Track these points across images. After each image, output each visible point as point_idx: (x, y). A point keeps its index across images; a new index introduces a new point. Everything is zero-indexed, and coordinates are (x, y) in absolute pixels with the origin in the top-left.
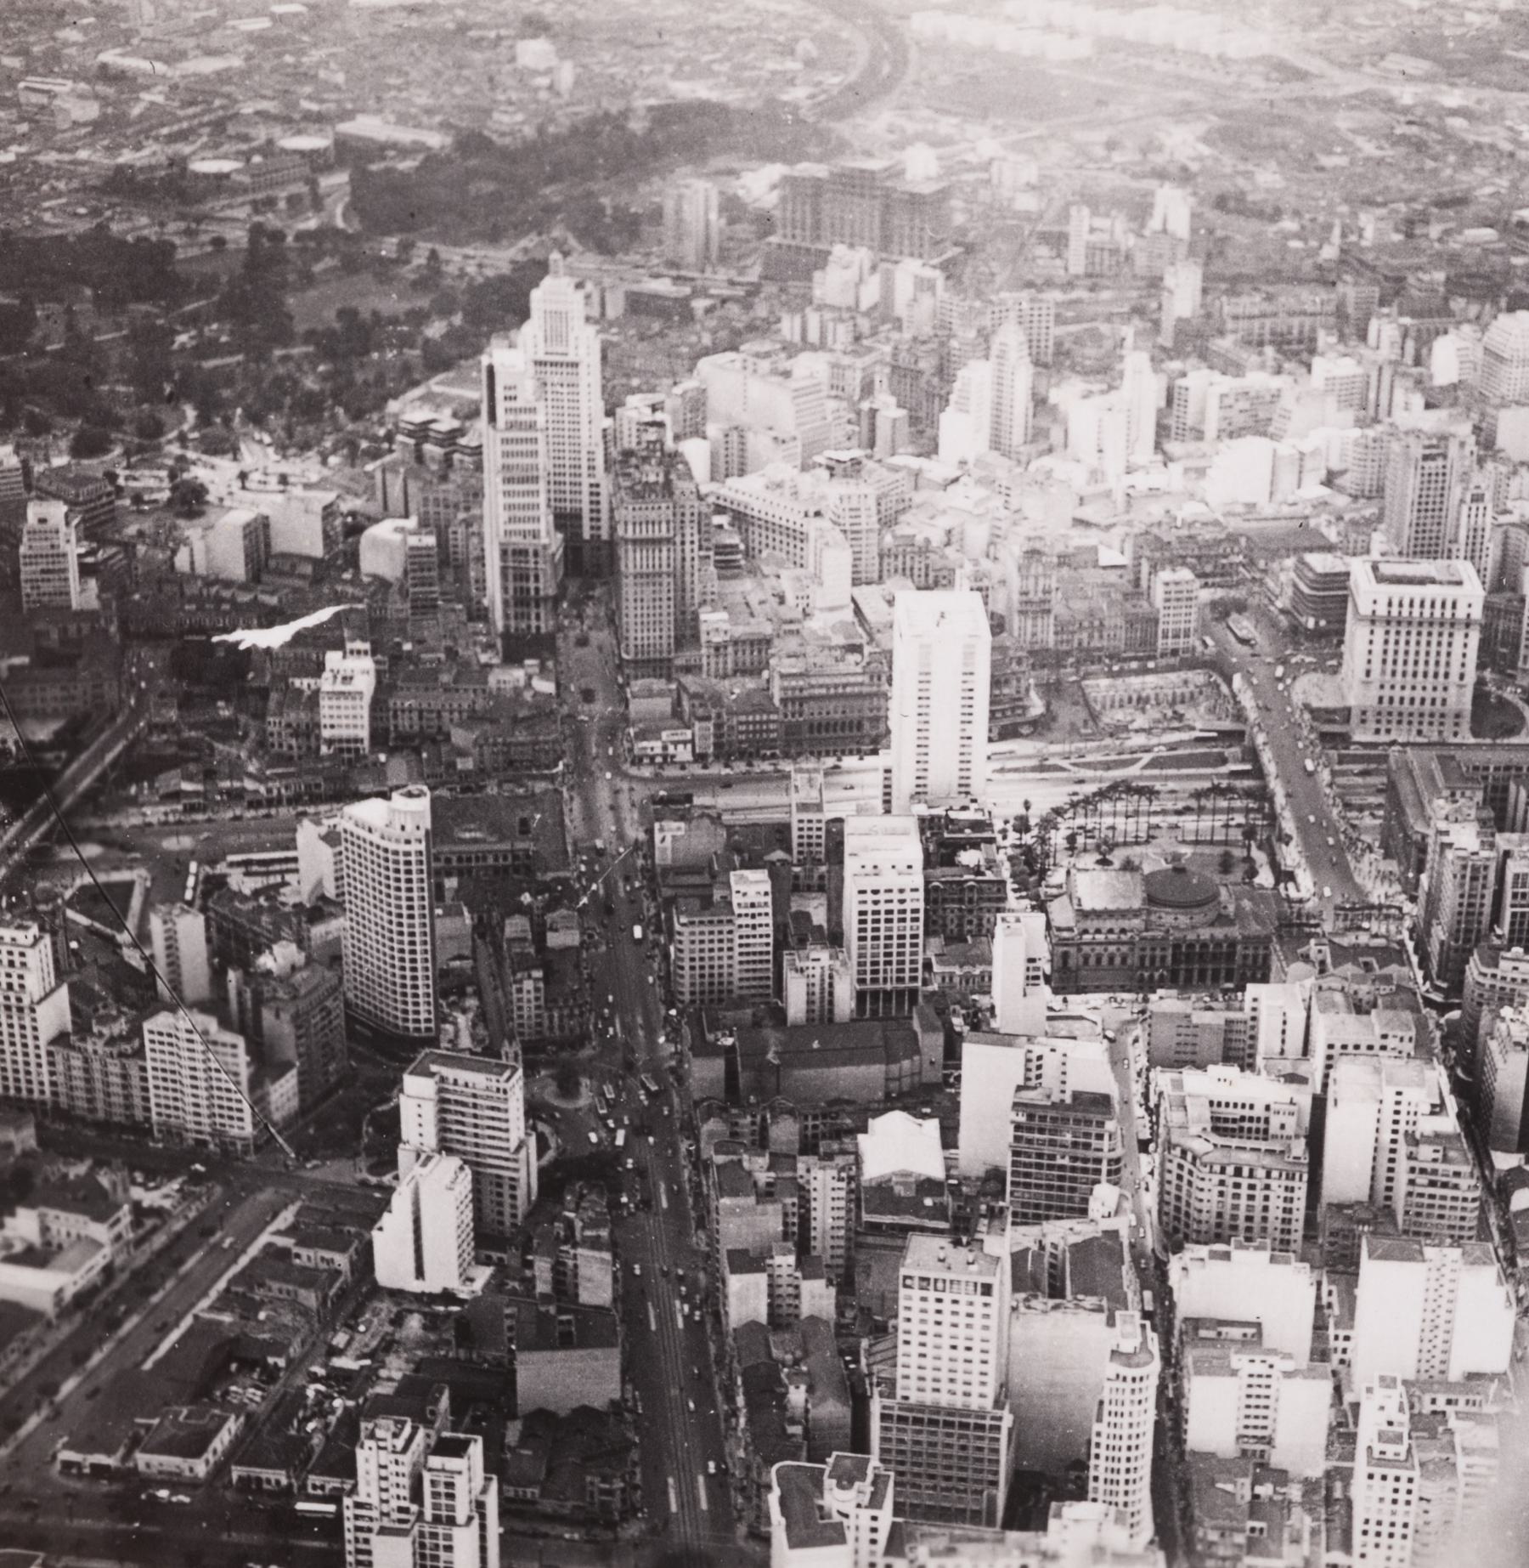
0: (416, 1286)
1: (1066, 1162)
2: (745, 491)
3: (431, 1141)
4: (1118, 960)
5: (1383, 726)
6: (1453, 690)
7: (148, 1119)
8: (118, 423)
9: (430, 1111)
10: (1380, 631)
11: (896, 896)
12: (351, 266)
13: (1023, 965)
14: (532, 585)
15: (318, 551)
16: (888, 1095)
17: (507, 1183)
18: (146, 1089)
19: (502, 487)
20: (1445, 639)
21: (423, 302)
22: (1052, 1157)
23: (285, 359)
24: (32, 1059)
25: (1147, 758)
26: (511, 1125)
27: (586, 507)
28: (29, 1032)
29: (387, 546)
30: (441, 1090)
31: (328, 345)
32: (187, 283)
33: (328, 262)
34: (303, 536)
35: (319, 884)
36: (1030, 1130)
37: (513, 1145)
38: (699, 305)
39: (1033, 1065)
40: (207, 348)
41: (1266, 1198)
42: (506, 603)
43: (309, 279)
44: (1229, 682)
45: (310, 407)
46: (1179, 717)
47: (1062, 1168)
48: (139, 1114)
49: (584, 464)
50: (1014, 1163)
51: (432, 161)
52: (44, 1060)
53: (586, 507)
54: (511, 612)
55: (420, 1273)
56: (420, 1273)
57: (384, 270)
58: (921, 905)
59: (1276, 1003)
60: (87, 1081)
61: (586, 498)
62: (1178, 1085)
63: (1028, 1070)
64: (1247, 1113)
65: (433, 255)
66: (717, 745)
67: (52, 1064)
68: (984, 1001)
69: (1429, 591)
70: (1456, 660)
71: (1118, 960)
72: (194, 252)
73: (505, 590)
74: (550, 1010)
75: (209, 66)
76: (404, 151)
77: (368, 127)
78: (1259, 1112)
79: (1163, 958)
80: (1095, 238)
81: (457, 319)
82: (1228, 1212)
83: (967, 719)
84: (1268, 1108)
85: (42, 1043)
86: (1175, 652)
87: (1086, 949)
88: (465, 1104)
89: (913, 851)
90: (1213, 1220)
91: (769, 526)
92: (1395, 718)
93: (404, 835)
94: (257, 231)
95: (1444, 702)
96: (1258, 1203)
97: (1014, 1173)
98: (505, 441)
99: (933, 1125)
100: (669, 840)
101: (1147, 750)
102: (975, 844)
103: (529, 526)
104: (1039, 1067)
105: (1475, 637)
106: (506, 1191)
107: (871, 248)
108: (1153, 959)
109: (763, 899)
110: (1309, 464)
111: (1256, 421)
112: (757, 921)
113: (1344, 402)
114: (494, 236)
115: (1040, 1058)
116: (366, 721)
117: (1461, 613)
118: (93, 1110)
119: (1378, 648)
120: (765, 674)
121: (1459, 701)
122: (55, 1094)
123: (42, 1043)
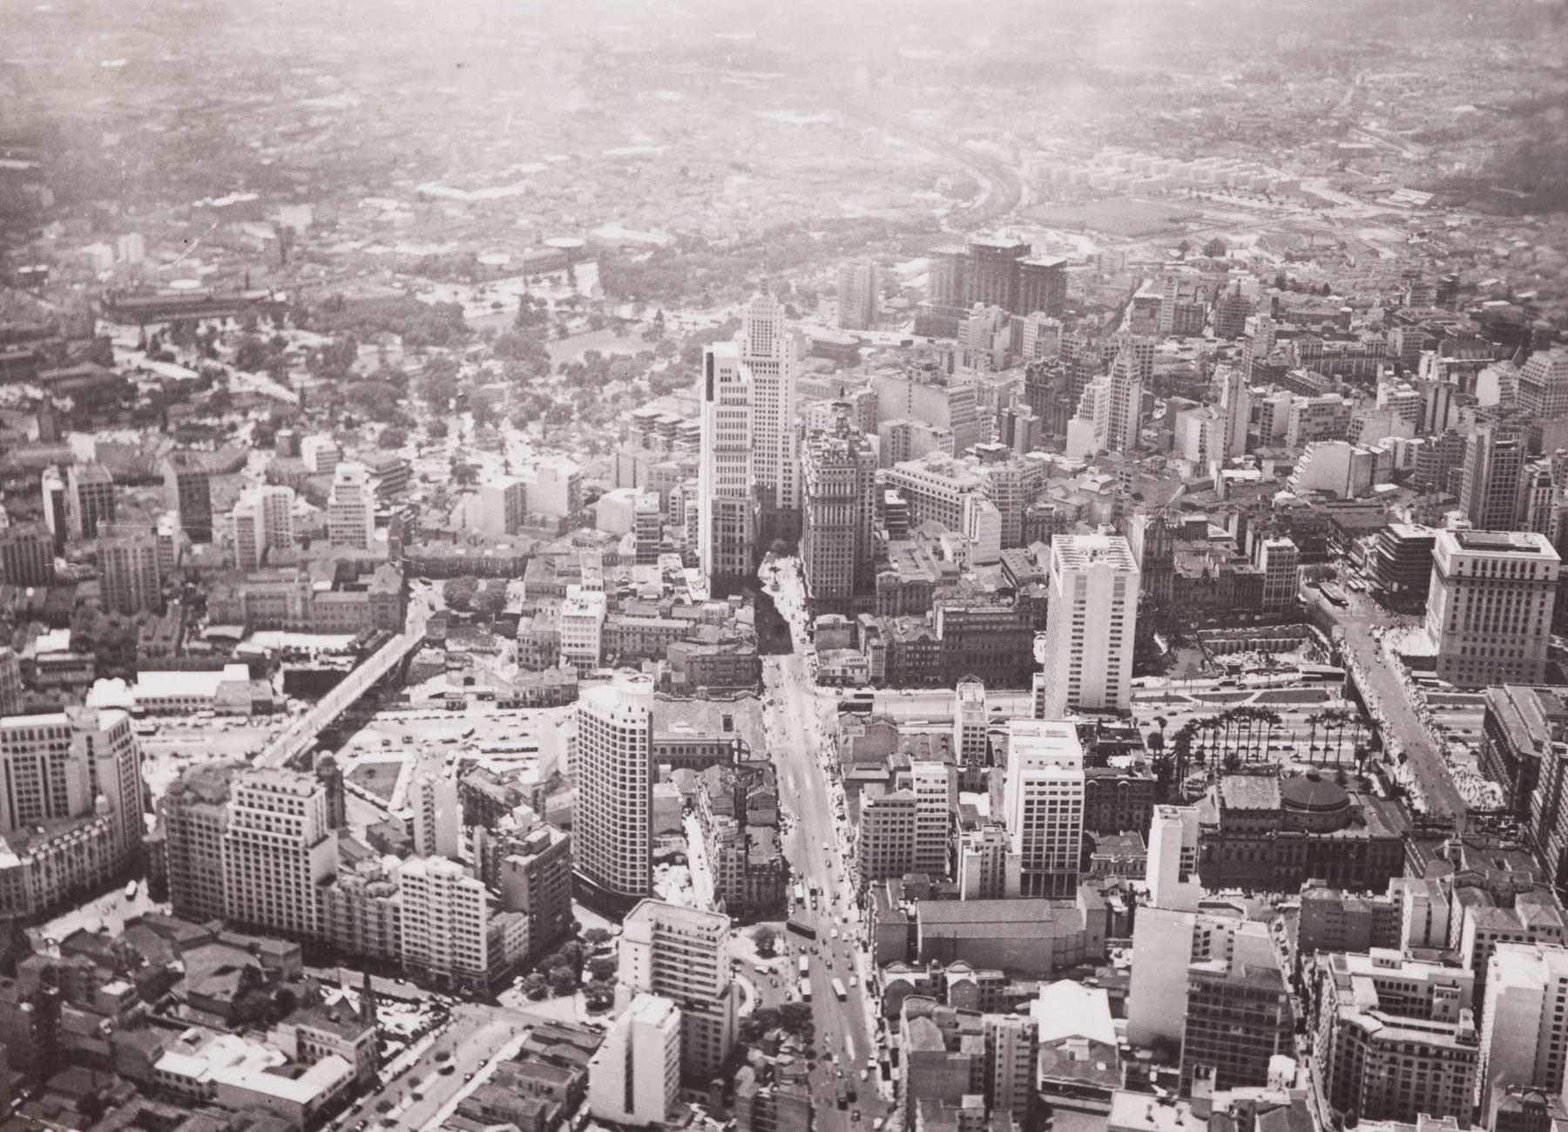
0: (628, 1119)
1: (1240, 1032)
2: (912, 469)
3: (645, 979)
4: (1257, 857)
5: (1465, 674)
6: (1530, 642)
7: (398, 955)
8: (413, 425)
9: (645, 954)
10: (1464, 591)
11: (1059, 788)
12: (597, 324)
13: (1178, 853)
14: (737, 534)
15: (565, 512)
16: (1054, 966)
17: (711, 1027)
18: (397, 928)
19: (715, 464)
20: (1524, 598)
21: (652, 347)
22: (1226, 1028)
23: (543, 385)
24: (304, 897)
25: (1258, 693)
26: (719, 972)
27: (780, 482)
28: (302, 873)
29: (623, 504)
30: (657, 936)
31: (576, 375)
32: (473, 332)
33: (579, 321)
34: (552, 502)
35: (555, 761)
36: (1206, 1000)
37: (719, 990)
38: (864, 351)
39: (1201, 940)
40: (484, 377)
41: (1437, 1077)
42: (715, 550)
43: (563, 333)
44: (1328, 634)
45: (561, 416)
46: (1271, 663)
47: (1236, 1038)
48: (391, 949)
49: (780, 446)
50: (1188, 1032)
51: (660, 253)
52: (313, 899)
53: (780, 482)
54: (720, 556)
55: (629, 1107)
56: (629, 1107)
57: (620, 325)
58: (1082, 797)
59: (1409, 895)
60: (350, 927)
61: (780, 474)
62: (1342, 965)
63: (1195, 945)
64: (1410, 994)
65: (659, 317)
66: (888, 671)
67: (319, 902)
68: (1139, 886)
69: (1511, 554)
70: (1534, 615)
71: (1257, 857)
72: (479, 313)
73: (715, 539)
74: (750, 877)
75: (496, 193)
76: (641, 249)
77: (611, 233)
78: (1422, 994)
79: (1299, 856)
80: (1182, 302)
81: (677, 360)
82: (1398, 1089)
83: (1115, 642)
84: (1430, 990)
85: (312, 883)
86: (1276, 609)
87: (1228, 844)
88: (675, 950)
89: (1075, 750)
90: (1384, 1097)
91: (928, 500)
92: (1476, 667)
93: (629, 717)
94: (526, 299)
95: (1521, 653)
96: (1429, 1081)
97: (1188, 1042)
98: (720, 415)
99: (1101, 996)
100: (850, 743)
101: (1258, 687)
102: (1123, 750)
103: (738, 486)
104: (1207, 943)
105: (1551, 597)
106: (711, 1034)
107: (1002, 305)
108: (1289, 856)
109: (941, 786)
110: (1380, 464)
111: (1337, 428)
112: (935, 806)
113: (1405, 417)
114: (707, 304)
115: (1207, 934)
116: (597, 642)
117: (1539, 575)
118: (352, 945)
119: (1462, 605)
120: (929, 614)
121: (1535, 653)
122: (321, 929)
123: (312, 883)
